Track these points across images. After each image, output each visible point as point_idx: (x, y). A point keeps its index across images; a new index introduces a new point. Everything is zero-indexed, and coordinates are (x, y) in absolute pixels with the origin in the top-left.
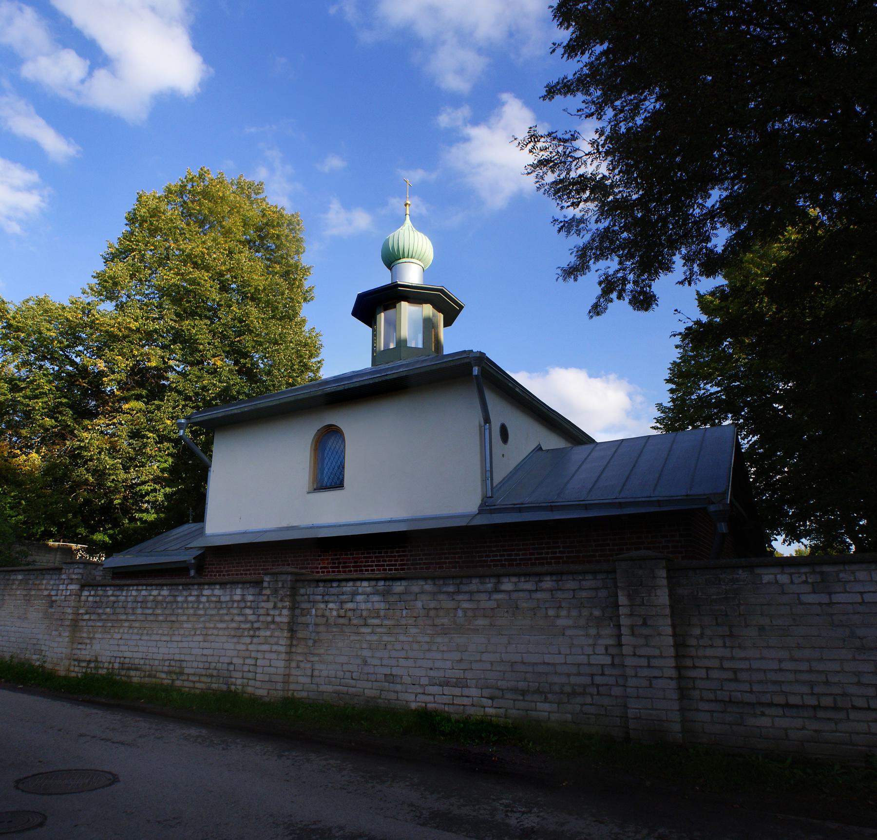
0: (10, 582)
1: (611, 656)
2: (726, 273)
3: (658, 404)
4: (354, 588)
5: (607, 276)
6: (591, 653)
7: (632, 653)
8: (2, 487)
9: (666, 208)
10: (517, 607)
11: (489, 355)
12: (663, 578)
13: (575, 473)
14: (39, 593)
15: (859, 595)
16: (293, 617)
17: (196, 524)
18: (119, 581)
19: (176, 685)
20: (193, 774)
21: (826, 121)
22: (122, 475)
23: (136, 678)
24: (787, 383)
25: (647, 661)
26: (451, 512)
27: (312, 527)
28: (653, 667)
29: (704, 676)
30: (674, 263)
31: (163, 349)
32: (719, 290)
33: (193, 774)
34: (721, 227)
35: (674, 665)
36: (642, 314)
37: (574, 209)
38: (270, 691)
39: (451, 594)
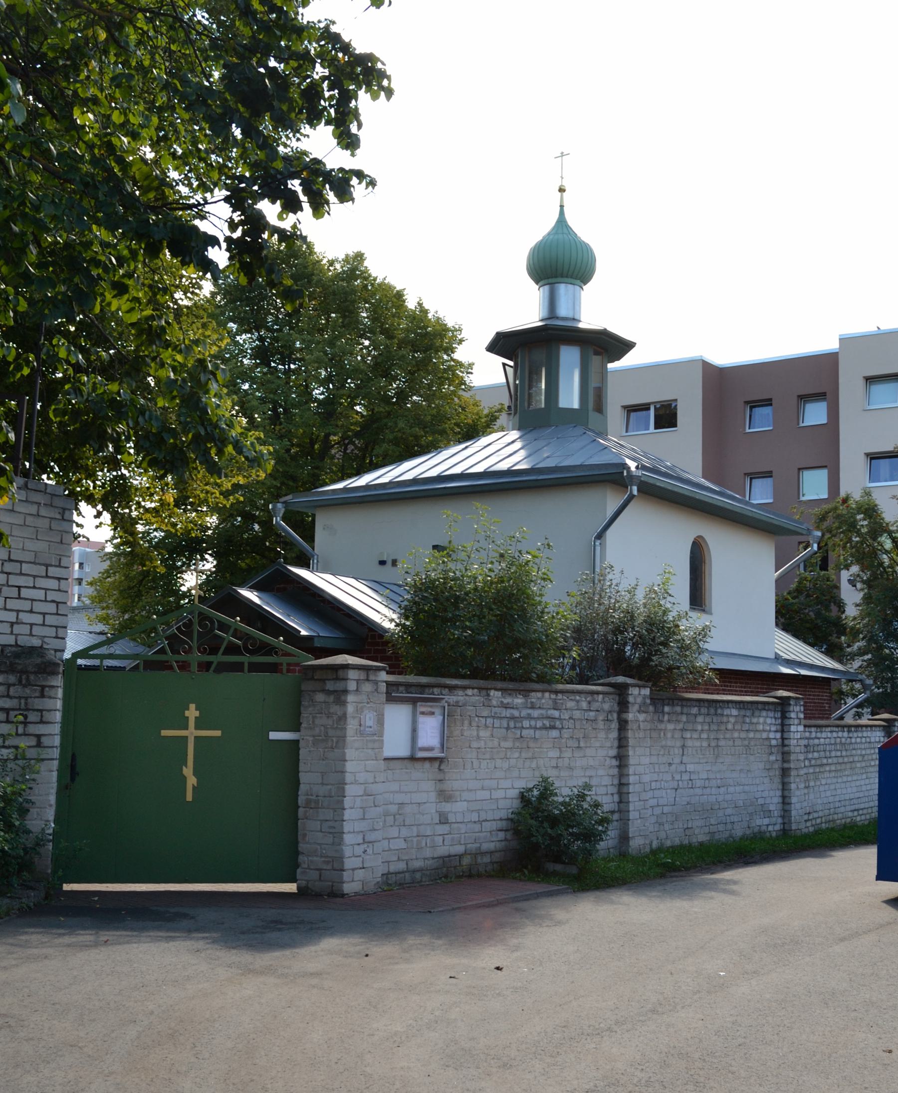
0: (725, 719)
1: (754, 409)
2: (240, 240)
3: (733, 893)
4: (44, 683)
5: (546, 790)
6: (14, 620)
7: (5, 720)
8: (2, 404)
9: (295, 415)
10: (51, 529)
11: (264, 211)
12: (304, 783)
13: (622, 743)
14: (758, 735)
15: (41, 617)
16: (782, 735)
17: (299, 510)
18: (448, 682)
19: (858, 566)
20: (778, 1034)
21: (85, 218)
22: (409, 431)
23: (426, 939)
24: (120, 171)
25: (5, 715)
26: (313, 948)
27: (710, 556)
28: (44, 565)
29: (35, 512)
30: (347, 256)
31: (317, 170)
32: (237, 127)
33: (778, 1034)
34: (334, 702)
35: (344, 885)
36: (320, 220)
37: (857, 605)
38: (59, 516)
39: (706, 704)
